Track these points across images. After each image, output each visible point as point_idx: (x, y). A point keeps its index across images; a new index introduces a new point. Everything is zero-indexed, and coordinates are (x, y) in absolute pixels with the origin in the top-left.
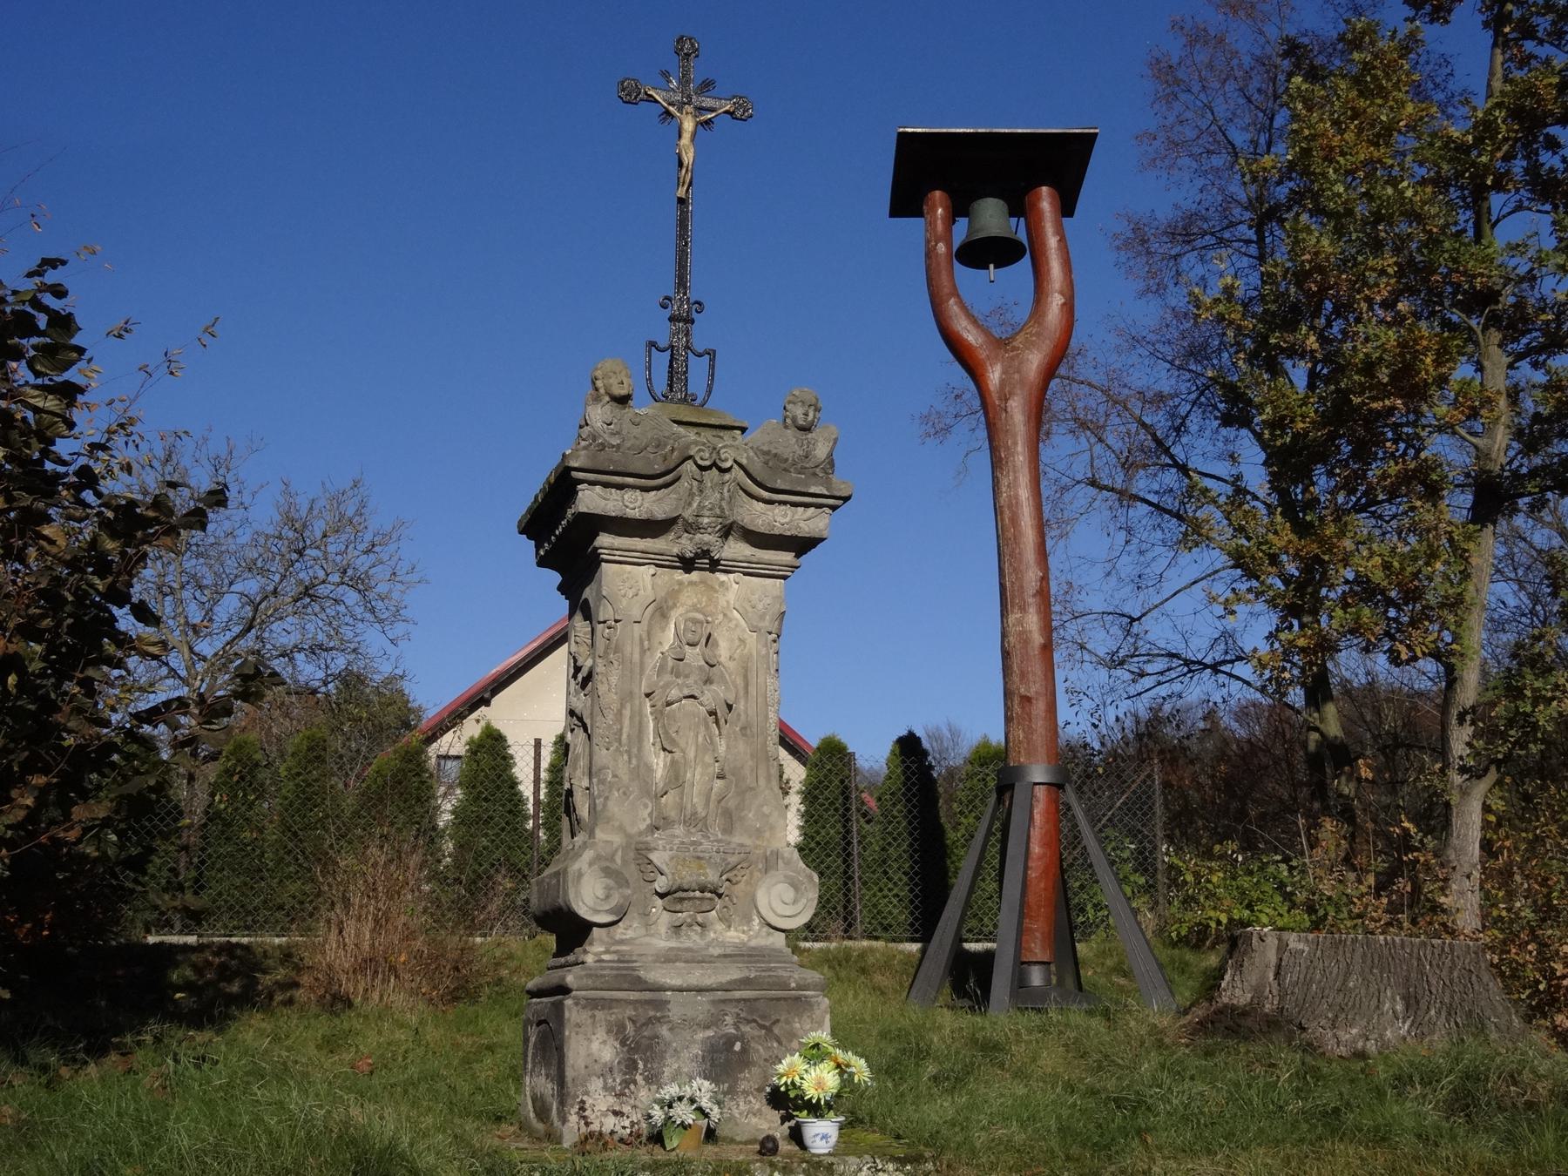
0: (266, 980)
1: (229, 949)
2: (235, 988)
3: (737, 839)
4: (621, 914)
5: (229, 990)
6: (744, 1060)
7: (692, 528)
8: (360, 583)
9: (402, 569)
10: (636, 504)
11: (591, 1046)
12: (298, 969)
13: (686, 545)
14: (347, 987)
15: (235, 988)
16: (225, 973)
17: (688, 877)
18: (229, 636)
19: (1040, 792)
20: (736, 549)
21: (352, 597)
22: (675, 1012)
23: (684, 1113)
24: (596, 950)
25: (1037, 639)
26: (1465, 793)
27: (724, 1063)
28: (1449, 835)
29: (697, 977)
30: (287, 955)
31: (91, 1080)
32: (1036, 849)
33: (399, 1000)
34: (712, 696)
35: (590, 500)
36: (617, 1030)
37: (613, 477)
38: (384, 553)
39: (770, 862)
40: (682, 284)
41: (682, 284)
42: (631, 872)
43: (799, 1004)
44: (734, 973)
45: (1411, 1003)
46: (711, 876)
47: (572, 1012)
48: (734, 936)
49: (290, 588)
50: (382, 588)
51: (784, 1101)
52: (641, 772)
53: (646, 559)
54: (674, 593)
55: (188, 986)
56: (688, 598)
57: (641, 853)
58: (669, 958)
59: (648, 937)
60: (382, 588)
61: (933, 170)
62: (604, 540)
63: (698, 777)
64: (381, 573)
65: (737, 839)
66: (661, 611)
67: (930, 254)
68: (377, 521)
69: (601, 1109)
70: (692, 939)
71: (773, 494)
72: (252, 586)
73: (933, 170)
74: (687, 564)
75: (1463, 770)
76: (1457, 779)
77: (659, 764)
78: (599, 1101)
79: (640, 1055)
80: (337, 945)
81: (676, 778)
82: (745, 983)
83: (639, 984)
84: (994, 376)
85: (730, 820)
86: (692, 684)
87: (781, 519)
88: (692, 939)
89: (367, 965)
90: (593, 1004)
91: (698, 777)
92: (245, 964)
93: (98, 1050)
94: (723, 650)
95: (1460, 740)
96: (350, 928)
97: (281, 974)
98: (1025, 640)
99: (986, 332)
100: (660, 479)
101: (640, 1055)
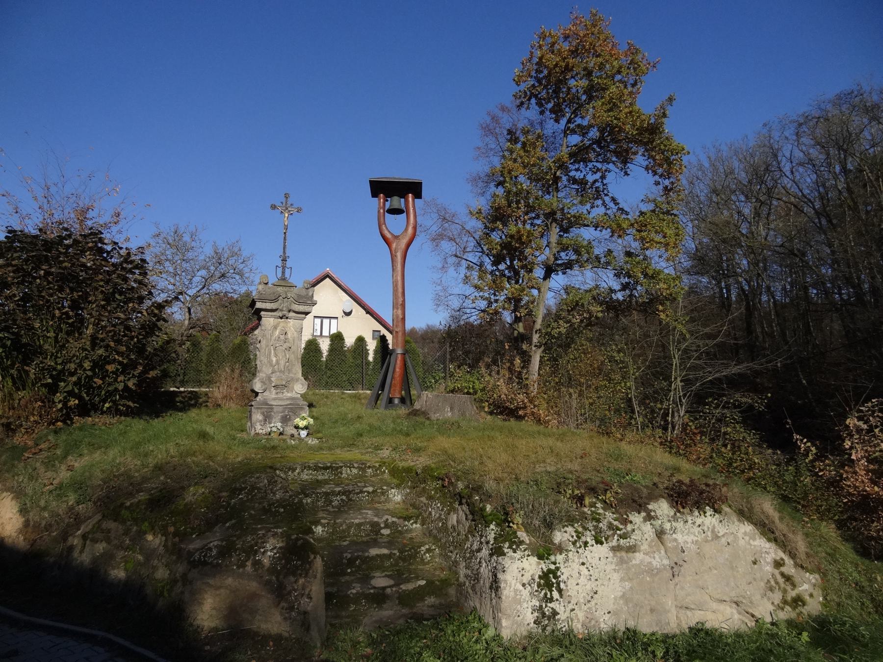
0: (201, 400)
1: (191, 392)
2: (193, 402)
3: (291, 375)
4: (265, 391)
5: (193, 401)
6: (290, 419)
7: (282, 310)
8: (241, 274)
9: (254, 268)
10: (269, 306)
11: (257, 416)
12: (209, 398)
13: (280, 314)
14: (220, 402)
15: (193, 402)
16: (190, 399)
17: (278, 383)
18: (198, 289)
19: (399, 356)
20: (292, 314)
21: (237, 277)
22: (275, 410)
23: (274, 429)
24: (259, 398)
25: (401, 317)
26: (535, 352)
27: (285, 420)
28: (130, 413)
29: (280, 403)
30: (206, 394)
31: (156, 422)
32: (398, 370)
33: (233, 405)
34: (286, 345)
35: (259, 305)
36: (263, 414)
37: (263, 300)
38: (248, 263)
39: (297, 380)
40: (284, 252)
41: (284, 252)
42: (267, 382)
43: (302, 409)
44: (288, 402)
45: (452, 409)
46: (284, 383)
47: (253, 410)
48: (289, 395)
49: (218, 274)
50: (247, 275)
51: (297, 427)
52: (270, 362)
53: (272, 317)
54: (279, 323)
55: (181, 402)
56: (282, 325)
57: (269, 378)
58: (275, 399)
59: (271, 395)
60: (247, 275)
61: (379, 188)
62: (262, 313)
63: (282, 363)
64: (246, 270)
65: (291, 375)
66: (275, 328)
67: (379, 211)
68: (245, 253)
69: (259, 429)
70: (280, 396)
71: (300, 303)
72: (203, 273)
73: (379, 188)
74: (281, 318)
75: (535, 346)
76: (534, 348)
77: (274, 359)
78: (258, 427)
79: (267, 418)
80: (217, 392)
81: (278, 362)
82: (290, 404)
83: (267, 404)
84: (394, 246)
85: (289, 371)
86: (281, 343)
87: (302, 308)
88: (280, 396)
89: (225, 397)
90: (258, 408)
91: (282, 363)
92: (195, 396)
93: (157, 417)
94: (289, 335)
95: (536, 338)
96: (221, 389)
97: (204, 399)
98: (397, 317)
99: (392, 234)
100: (275, 300)
101: (267, 418)
